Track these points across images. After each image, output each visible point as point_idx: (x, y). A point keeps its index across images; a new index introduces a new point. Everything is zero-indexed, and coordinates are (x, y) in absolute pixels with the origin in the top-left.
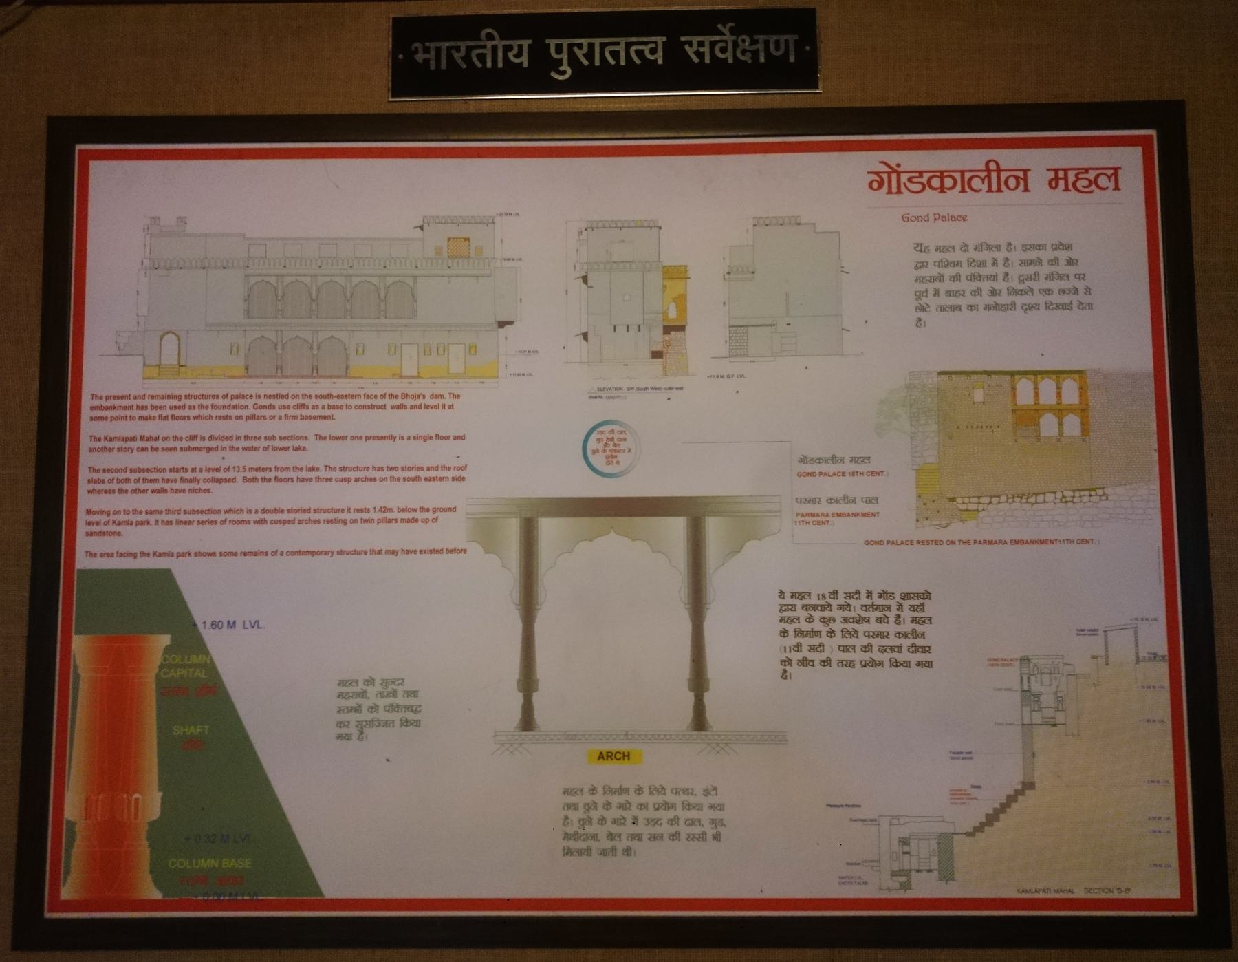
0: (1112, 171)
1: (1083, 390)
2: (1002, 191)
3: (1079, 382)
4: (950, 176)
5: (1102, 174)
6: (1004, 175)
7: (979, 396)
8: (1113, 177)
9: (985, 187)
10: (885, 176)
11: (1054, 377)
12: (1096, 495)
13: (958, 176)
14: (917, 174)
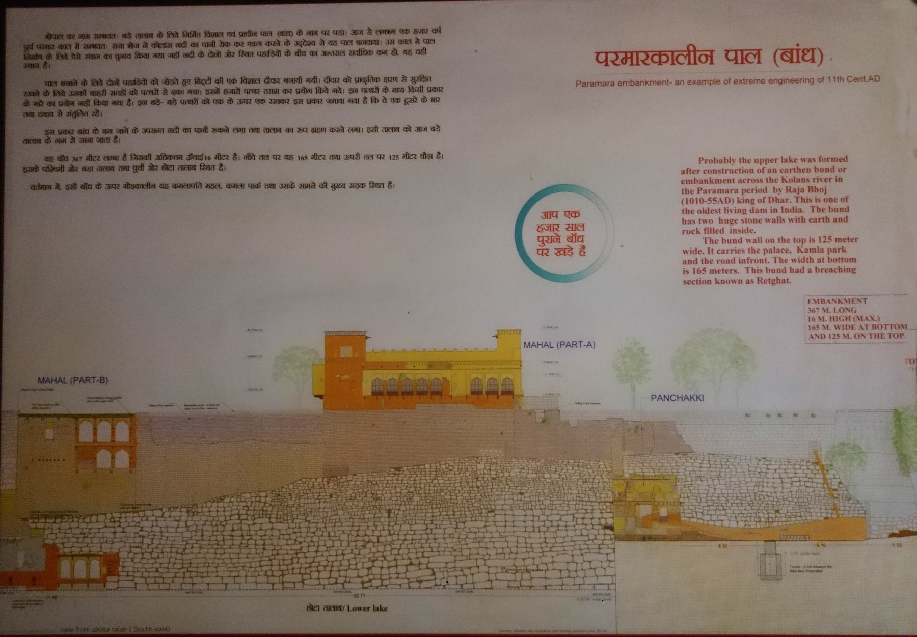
0: (756, 52)
1: (132, 430)
3: (129, 423)
4: (666, 55)
5: (679, 55)
6: (698, 54)
7: (49, 434)
8: (757, 56)
9: (686, 61)
11: (110, 419)
12: (139, 516)
13: (670, 54)
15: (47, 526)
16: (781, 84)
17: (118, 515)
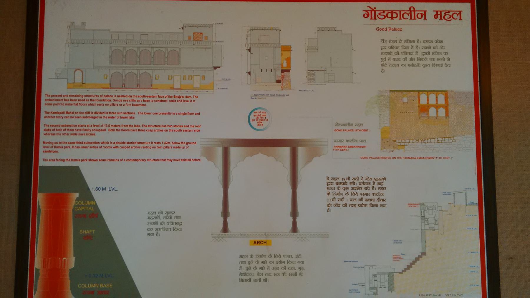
0: (459, 12)
2: (402, 19)
3: (444, 95)
6: (416, 13)
7: (405, 100)
9: (409, 17)
10: (370, 12)
11: (435, 93)
12: (451, 140)
13: (398, 13)
14: (382, 12)
15: (406, 144)
16: (103, 142)
17: (441, 139)
